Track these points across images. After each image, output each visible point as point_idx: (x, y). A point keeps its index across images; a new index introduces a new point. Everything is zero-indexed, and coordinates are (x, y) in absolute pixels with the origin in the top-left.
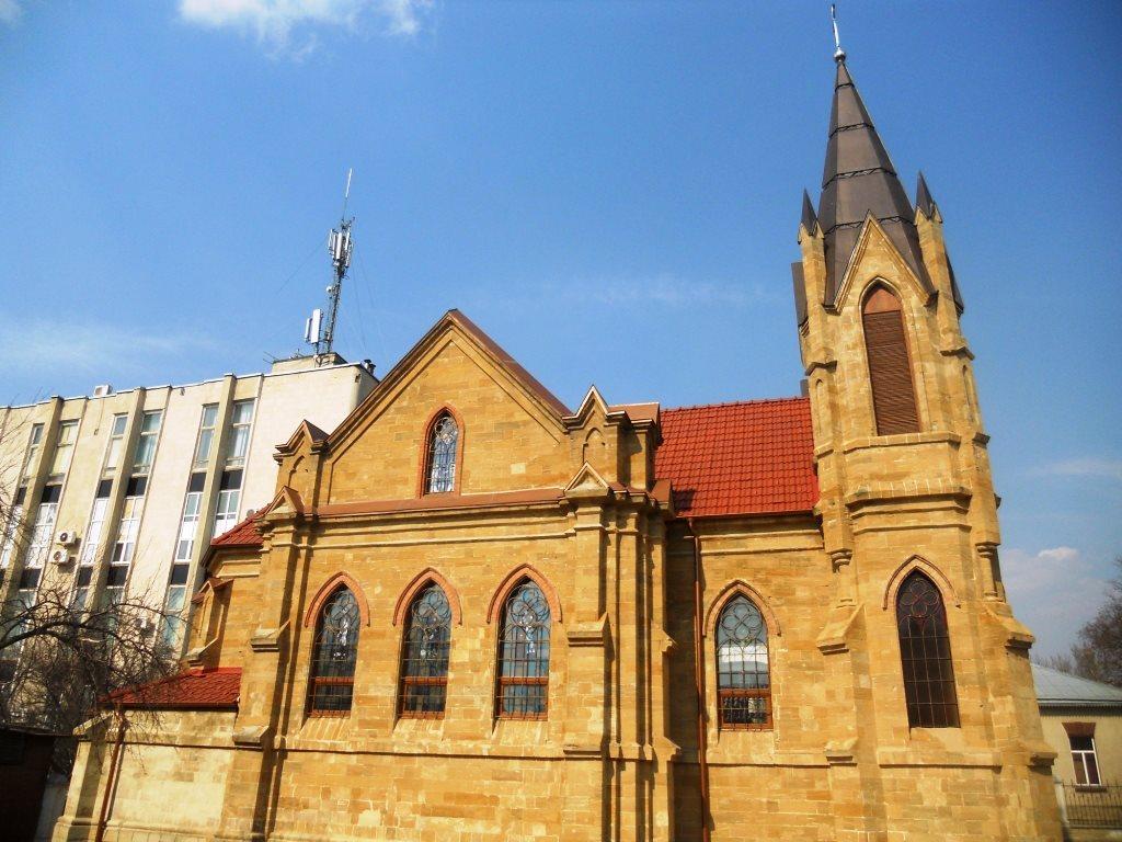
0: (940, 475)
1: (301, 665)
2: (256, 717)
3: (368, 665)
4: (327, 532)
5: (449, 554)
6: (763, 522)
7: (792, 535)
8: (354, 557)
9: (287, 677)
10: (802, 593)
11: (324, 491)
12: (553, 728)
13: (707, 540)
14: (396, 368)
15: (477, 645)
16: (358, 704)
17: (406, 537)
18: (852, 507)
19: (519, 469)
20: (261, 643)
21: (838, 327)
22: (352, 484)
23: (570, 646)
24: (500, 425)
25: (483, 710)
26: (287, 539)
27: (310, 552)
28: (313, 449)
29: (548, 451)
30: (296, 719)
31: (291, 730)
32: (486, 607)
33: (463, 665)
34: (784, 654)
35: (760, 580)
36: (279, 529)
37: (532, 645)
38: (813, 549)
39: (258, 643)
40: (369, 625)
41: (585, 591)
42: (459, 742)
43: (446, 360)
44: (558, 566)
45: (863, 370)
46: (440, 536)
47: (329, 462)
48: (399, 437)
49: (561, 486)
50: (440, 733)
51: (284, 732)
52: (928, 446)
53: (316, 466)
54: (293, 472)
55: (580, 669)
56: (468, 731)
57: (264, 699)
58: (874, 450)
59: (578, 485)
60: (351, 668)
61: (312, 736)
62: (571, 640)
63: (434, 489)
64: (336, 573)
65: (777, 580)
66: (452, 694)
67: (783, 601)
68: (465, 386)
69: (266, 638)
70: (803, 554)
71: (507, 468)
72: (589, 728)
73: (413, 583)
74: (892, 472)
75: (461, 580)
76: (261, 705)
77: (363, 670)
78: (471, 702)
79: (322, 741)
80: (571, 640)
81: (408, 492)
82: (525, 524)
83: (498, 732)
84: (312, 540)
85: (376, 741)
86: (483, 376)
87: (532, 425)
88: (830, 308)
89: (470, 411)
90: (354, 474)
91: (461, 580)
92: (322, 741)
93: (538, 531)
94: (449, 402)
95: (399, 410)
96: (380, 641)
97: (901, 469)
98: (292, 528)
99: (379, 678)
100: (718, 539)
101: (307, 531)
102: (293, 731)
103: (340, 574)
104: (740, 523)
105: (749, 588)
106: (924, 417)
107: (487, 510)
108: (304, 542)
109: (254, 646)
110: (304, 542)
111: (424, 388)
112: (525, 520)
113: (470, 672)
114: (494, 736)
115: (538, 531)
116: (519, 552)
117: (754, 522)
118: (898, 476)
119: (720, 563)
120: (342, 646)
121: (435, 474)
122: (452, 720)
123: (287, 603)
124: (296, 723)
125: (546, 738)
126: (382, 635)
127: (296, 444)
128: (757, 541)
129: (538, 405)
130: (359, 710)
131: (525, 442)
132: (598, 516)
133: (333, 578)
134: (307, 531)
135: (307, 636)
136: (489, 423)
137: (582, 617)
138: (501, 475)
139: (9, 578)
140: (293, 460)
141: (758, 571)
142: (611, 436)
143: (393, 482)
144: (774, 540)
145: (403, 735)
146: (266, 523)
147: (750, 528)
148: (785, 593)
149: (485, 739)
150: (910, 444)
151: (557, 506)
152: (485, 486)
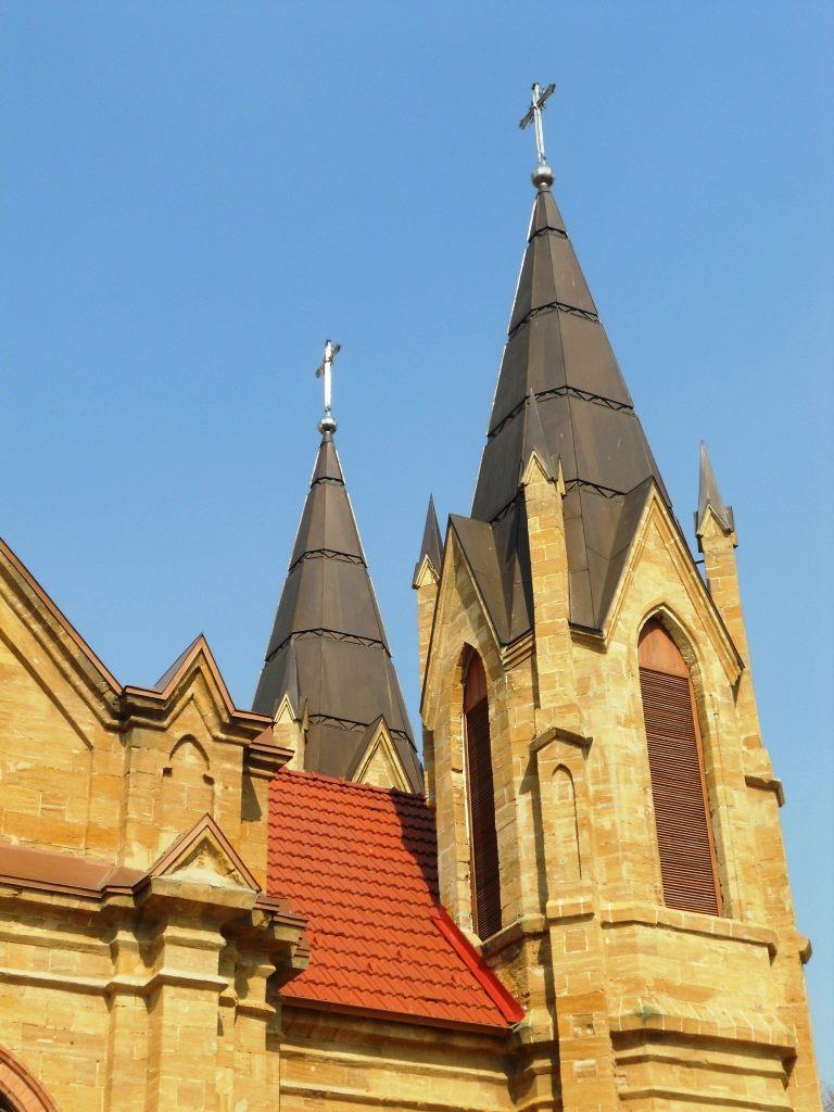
0: (759, 1009)
6: (412, 1036)
7: (456, 1076)
18: (620, 1039)
21: (599, 676)
29: (59, 760)
44: (76, 1067)
45: (641, 774)
49: (139, 862)
52: (741, 946)
58: (661, 932)
74: (688, 983)
87: (18, 682)
88: (589, 635)
97: (702, 981)
104: (366, 1029)
106: (735, 891)
117: (394, 1033)
118: (700, 995)
132: (215, 957)
139: (292, 736)
142: (228, 766)
147: (377, 1045)
150: (715, 937)
151: (94, 907)
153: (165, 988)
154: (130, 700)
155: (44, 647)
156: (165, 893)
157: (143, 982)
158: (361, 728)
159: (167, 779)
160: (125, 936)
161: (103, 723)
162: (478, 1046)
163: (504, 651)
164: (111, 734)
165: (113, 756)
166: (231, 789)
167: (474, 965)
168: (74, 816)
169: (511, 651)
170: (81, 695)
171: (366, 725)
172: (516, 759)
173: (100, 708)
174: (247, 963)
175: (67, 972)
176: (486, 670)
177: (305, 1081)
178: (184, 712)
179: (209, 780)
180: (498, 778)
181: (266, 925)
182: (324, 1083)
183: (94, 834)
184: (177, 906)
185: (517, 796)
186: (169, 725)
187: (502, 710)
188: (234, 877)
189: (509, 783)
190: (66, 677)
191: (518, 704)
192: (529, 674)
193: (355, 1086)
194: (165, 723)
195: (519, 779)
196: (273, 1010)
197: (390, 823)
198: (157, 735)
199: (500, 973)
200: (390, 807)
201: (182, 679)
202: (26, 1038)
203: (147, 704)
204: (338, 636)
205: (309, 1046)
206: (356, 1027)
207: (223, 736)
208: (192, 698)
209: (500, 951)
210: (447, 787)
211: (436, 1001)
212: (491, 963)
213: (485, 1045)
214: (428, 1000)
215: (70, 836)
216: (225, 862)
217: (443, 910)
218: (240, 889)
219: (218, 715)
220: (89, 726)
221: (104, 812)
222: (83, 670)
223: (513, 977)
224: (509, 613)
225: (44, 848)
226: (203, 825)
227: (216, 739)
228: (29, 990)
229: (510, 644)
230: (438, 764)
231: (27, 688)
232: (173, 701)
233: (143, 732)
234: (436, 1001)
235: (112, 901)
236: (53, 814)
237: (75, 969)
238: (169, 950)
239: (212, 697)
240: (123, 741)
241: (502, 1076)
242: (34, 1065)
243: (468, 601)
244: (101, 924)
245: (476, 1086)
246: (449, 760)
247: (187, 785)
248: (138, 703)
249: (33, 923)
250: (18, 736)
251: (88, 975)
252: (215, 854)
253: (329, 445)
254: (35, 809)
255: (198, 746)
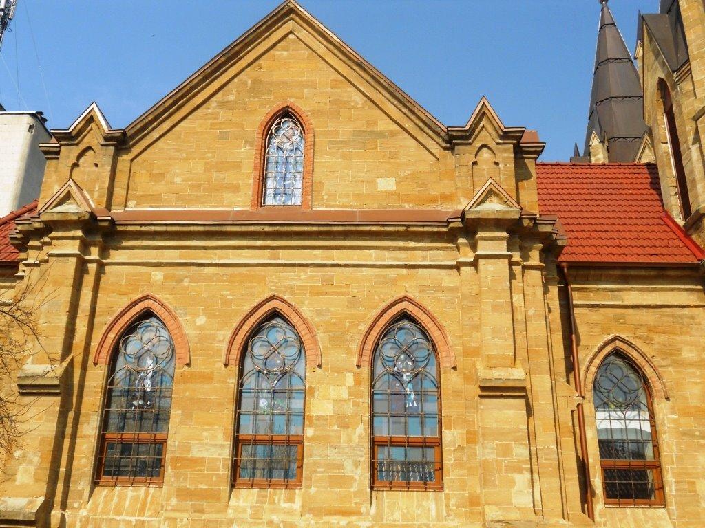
1: (88, 415)
2: (21, 486)
3: (188, 416)
4: (125, 243)
5: (299, 279)
6: (643, 273)
7: (672, 290)
8: (166, 278)
9: (69, 430)
10: (688, 354)
11: (119, 192)
12: (453, 501)
13: (579, 290)
14: (222, 54)
15: (345, 394)
16: (174, 468)
17: (239, 256)
19: (387, 184)
20: (37, 383)
22: (160, 187)
23: (481, 396)
24: (359, 133)
25: (357, 477)
26: (73, 247)
27: (101, 266)
28: (106, 139)
29: (426, 168)
30: (80, 488)
31: (73, 502)
32: (355, 347)
33: (325, 418)
34: (674, 421)
35: (640, 337)
36: (59, 234)
37: (412, 397)
38: (697, 306)
39: (28, 382)
40: (188, 365)
41: (495, 331)
42: (325, 519)
43: (285, 53)
44: (446, 301)
46: (286, 257)
47: (125, 158)
48: (224, 136)
49: (463, 204)
50: (297, 505)
51: (64, 506)
53: (110, 160)
54: (76, 165)
55: (495, 425)
56: (336, 505)
57: (36, 459)
59: (479, 204)
60: (161, 418)
61: (103, 512)
62: (483, 388)
63: (270, 201)
64: (139, 296)
65: (659, 339)
66: (312, 455)
67: (669, 362)
68: (313, 85)
69: (43, 376)
70: (686, 311)
71: (372, 183)
72: (513, 501)
73: (251, 314)
75: (319, 312)
76: (32, 469)
77: (182, 423)
78: (340, 466)
79: (122, 517)
80: (483, 388)
81: (238, 203)
82: (400, 249)
83: (377, 505)
84: (104, 252)
85: (205, 516)
86: (335, 76)
87: (400, 137)
89: (317, 113)
90: (162, 175)
91: (319, 312)
92: (122, 517)
93: (418, 258)
94: (293, 100)
95: (223, 105)
96: (206, 386)
98: (79, 233)
99: (205, 434)
100: (590, 290)
101: (99, 239)
102: (76, 505)
103: (146, 298)
104: (617, 272)
105: (630, 345)
107: (353, 229)
108: (94, 253)
109: (21, 386)
110: (94, 253)
111: (256, 82)
112: (401, 244)
113: (335, 427)
114: (373, 511)
115: (418, 258)
116: (395, 282)
117: (632, 272)
119: (595, 316)
120: (145, 391)
121: (271, 184)
122: (313, 490)
123: (70, 331)
124: (81, 494)
125: (445, 513)
126: (208, 378)
127: (80, 132)
128: (634, 295)
129: (410, 114)
130: (177, 476)
131: (393, 155)
132: (504, 243)
133: (136, 303)
134: (99, 239)
135: (96, 378)
136: (346, 129)
137: (493, 362)
138: (365, 189)
140: (76, 151)
141: (638, 327)
142: (506, 155)
143: (220, 188)
144: (654, 294)
145: (244, 510)
146: (37, 225)
147: (625, 279)
148: (669, 352)
149: (361, 514)
151: (445, 229)
152: (345, 200)
153: (480, 260)
154: (450, 133)
155: (410, 118)
156: (473, 217)
157: (472, 260)
158: (637, 140)
159: (475, 167)
160: (461, 240)
161: (442, 147)
162: (683, 274)
163: (675, 74)
164: (447, 152)
165: (449, 161)
166: (508, 165)
167: (681, 235)
168: (434, 191)
169: (678, 74)
170: (430, 137)
171: (640, 138)
172: (688, 128)
173: (440, 140)
174: (527, 245)
175: (437, 260)
176: (669, 88)
177: (588, 300)
178: (480, 134)
179: (497, 163)
180: (681, 140)
181: (531, 225)
182: (598, 301)
183: (446, 198)
184: (482, 223)
185: (691, 146)
186: (473, 142)
187: (679, 105)
188: (508, 205)
189: (686, 141)
190: (422, 130)
191: (686, 100)
192: (691, 83)
193: (616, 300)
194: (470, 141)
195: (691, 138)
196: (544, 265)
197: (645, 177)
198: (468, 148)
199: (694, 237)
200: (646, 171)
201: (475, 119)
202: (420, 292)
203: (459, 134)
204: (636, 99)
205: (588, 284)
206: (611, 272)
207: (501, 142)
208: (483, 127)
209: (692, 225)
210: (661, 152)
211: (657, 255)
212: (689, 233)
213: (687, 273)
214: (652, 255)
215: (433, 200)
216: (502, 198)
217: (666, 212)
218: (511, 209)
219: (497, 132)
220: (436, 149)
221: (446, 187)
222: (428, 125)
223: (700, 237)
224: (677, 54)
225: (421, 208)
226: (488, 183)
227: (498, 144)
228: (420, 270)
229: (678, 70)
230: (656, 141)
231: (405, 138)
232: (472, 130)
233: (460, 147)
234: (657, 255)
235: (451, 225)
236: (424, 192)
237: (441, 258)
238: (480, 243)
239: (493, 125)
240: (453, 153)
241: (700, 287)
242: (425, 303)
243: (657, 55)
244: (450, 236)
245: (685, 293)
246: (659, 139)
247: (486, 168)
248: (454, 134)
249: (419, 241)
250: (403, 160)
251: (448, 260)
252: (497, 195)
253: (605, 9)
254: (413, 190)
255: (489, 148)
